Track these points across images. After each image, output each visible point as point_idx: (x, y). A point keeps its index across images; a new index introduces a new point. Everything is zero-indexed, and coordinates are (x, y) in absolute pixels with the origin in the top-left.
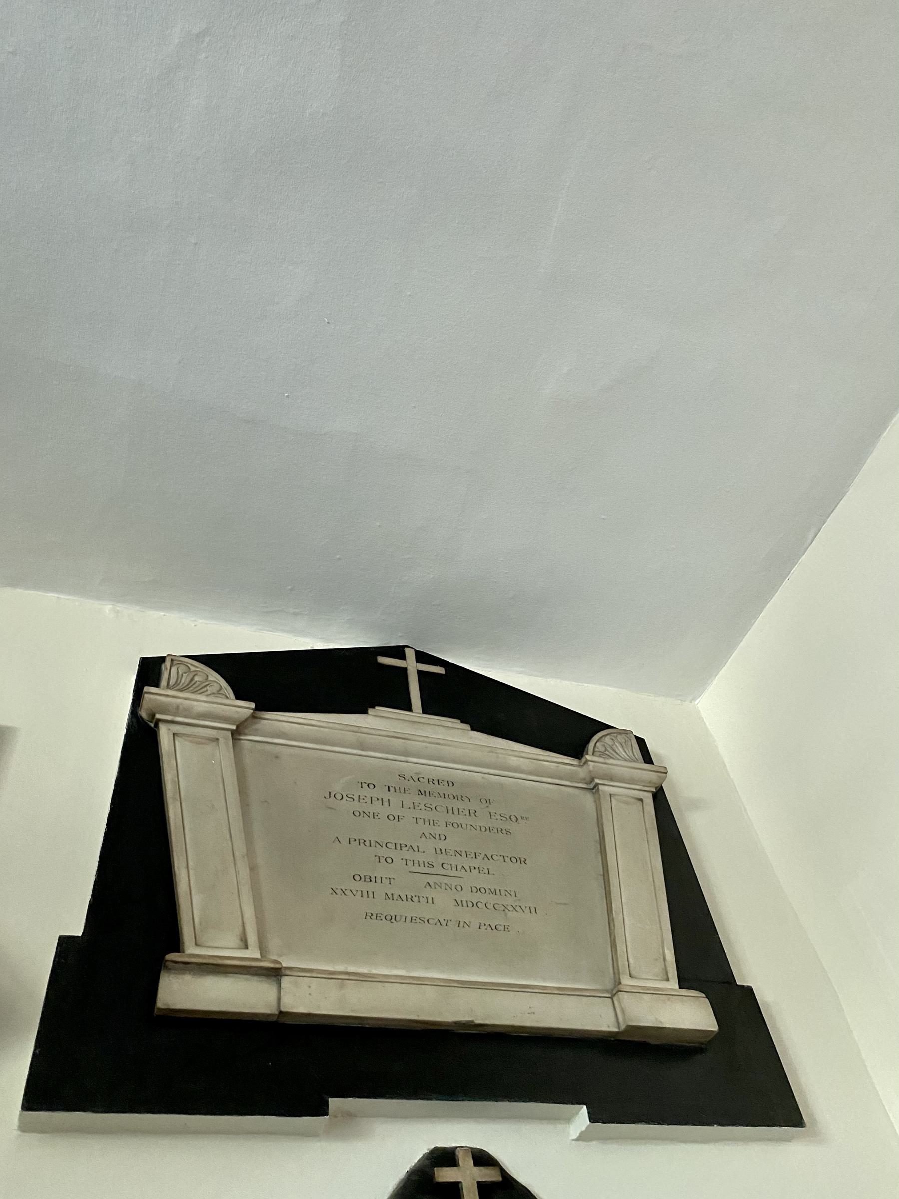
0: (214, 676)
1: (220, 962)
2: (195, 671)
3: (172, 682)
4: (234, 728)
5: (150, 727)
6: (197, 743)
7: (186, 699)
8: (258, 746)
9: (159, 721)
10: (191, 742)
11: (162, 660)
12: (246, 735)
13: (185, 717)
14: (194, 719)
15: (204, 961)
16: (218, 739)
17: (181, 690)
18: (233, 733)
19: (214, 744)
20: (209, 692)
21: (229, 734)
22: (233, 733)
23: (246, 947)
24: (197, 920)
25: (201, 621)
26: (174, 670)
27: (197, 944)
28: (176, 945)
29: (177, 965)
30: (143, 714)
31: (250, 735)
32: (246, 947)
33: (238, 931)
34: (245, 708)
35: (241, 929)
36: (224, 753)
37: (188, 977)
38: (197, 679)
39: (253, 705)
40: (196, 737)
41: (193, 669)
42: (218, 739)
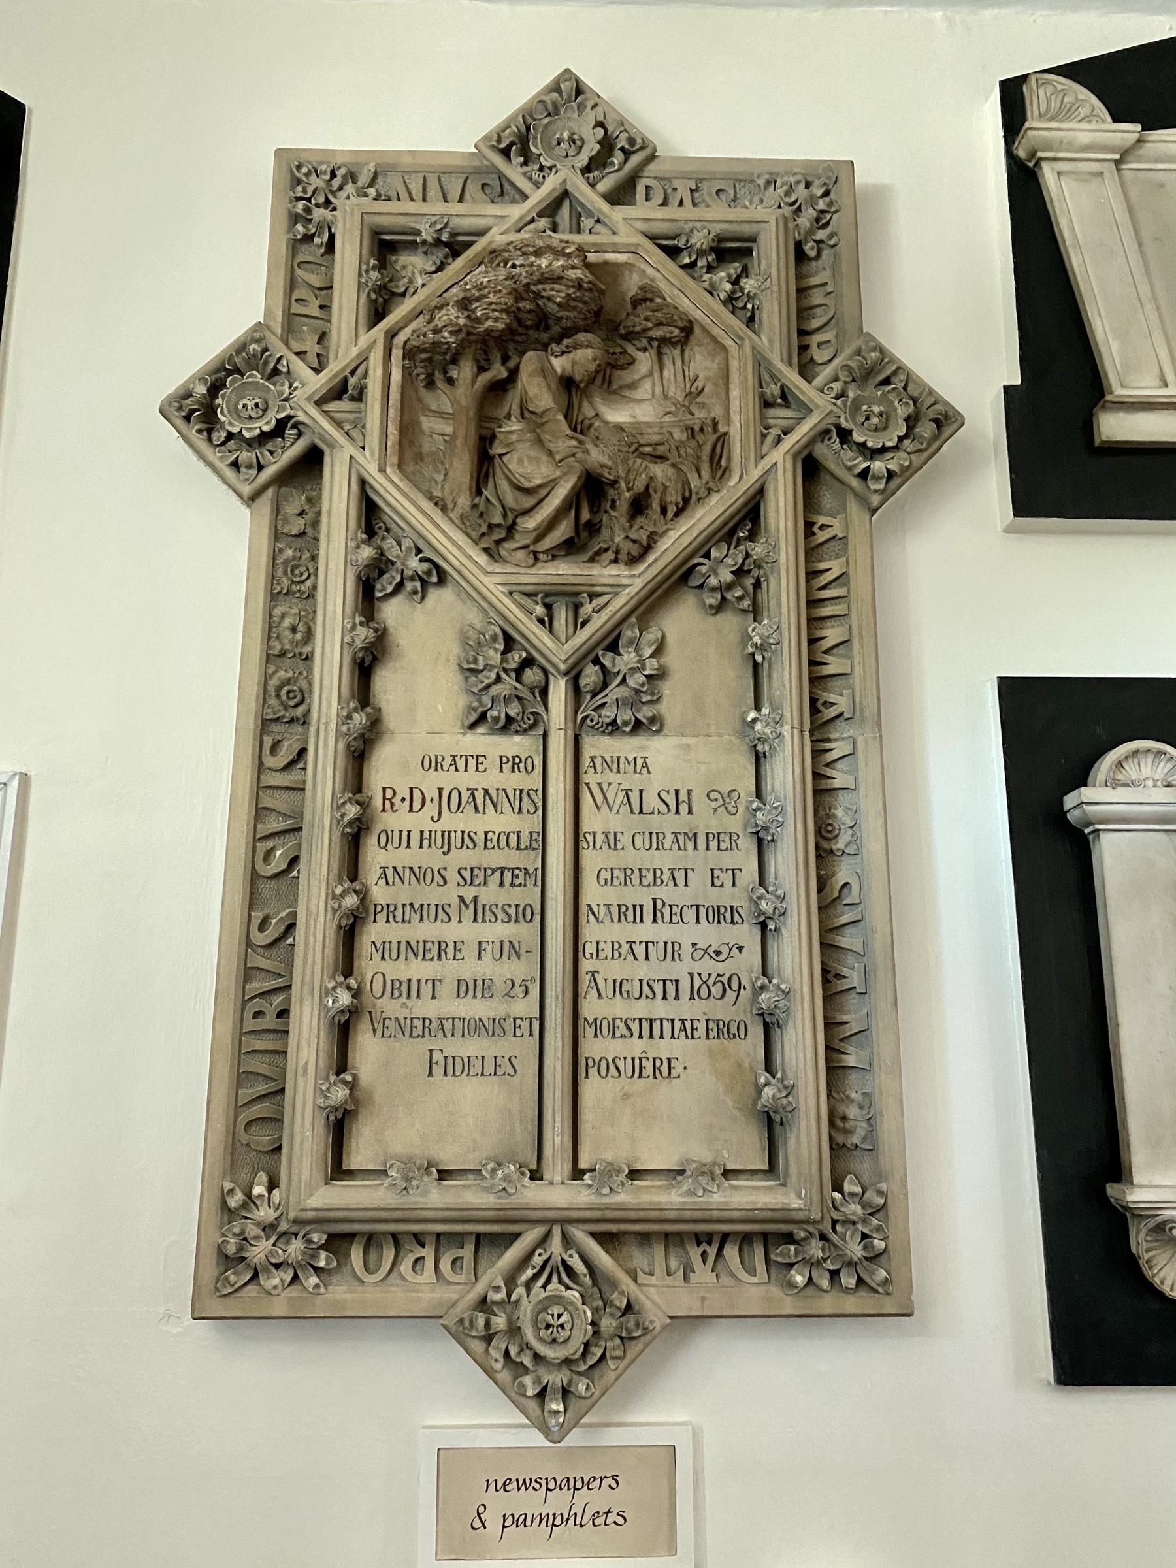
0: (1083, 93)
1: (1152, 400)
2: (1063, 90)
3: (1043, 109)
4: (1117, 157)
5: (1028, 167)
6: (1083, 181)
7: (1070, 130)
8: (1142, 174)
9: (1041, 159)
10: (1076, 180)
11: (1024, 78)
12: (1127, 162)
13: (1068, 151)
14: (1077, 152)
15: (1135, 400)
16: (1102, 173)
17: (1052, 119)
18: (1117, 163)
19: (1099, 179)
20: (1082, 116)
21: (1113, 166)
22: (1117, 163)
23: (1166, 386)
24: (1118, 366)
25: (1038, 13)
26: (1041, 91)
27: (1122, 386)
28: (1102, 395)
29: (1114, 405)
30: (1021, 153)
31: (1131, 162)
32: (1166, 386)
33: (1157, 371)
34: (1129, 131)
35: (1159, 371)
36: (1110, 187)
37: (1121, 415)
38: (1066, 100)
39: (1139, 127)
40: (1081, 173)
41: (1059, 87)
42: (1102, 173)
